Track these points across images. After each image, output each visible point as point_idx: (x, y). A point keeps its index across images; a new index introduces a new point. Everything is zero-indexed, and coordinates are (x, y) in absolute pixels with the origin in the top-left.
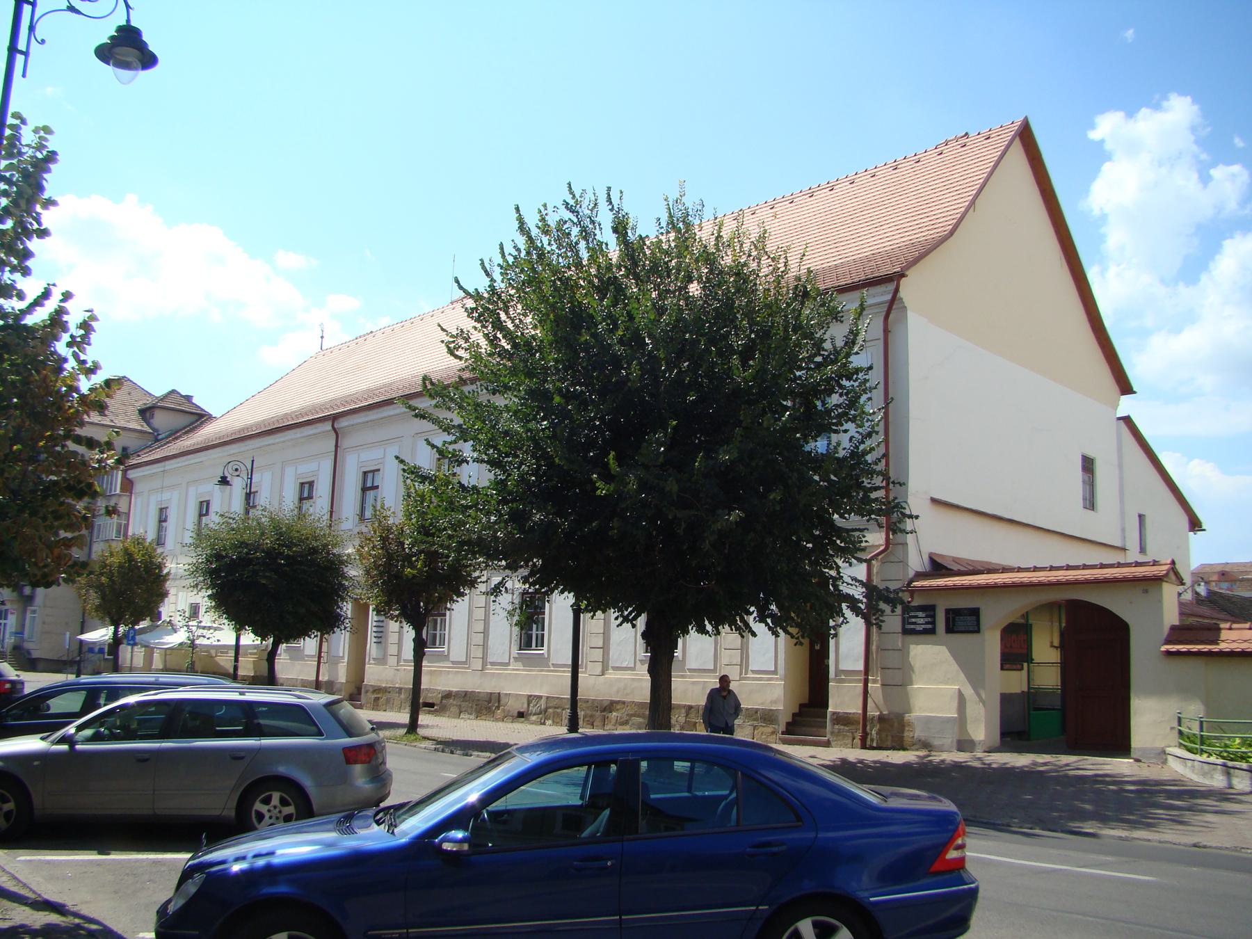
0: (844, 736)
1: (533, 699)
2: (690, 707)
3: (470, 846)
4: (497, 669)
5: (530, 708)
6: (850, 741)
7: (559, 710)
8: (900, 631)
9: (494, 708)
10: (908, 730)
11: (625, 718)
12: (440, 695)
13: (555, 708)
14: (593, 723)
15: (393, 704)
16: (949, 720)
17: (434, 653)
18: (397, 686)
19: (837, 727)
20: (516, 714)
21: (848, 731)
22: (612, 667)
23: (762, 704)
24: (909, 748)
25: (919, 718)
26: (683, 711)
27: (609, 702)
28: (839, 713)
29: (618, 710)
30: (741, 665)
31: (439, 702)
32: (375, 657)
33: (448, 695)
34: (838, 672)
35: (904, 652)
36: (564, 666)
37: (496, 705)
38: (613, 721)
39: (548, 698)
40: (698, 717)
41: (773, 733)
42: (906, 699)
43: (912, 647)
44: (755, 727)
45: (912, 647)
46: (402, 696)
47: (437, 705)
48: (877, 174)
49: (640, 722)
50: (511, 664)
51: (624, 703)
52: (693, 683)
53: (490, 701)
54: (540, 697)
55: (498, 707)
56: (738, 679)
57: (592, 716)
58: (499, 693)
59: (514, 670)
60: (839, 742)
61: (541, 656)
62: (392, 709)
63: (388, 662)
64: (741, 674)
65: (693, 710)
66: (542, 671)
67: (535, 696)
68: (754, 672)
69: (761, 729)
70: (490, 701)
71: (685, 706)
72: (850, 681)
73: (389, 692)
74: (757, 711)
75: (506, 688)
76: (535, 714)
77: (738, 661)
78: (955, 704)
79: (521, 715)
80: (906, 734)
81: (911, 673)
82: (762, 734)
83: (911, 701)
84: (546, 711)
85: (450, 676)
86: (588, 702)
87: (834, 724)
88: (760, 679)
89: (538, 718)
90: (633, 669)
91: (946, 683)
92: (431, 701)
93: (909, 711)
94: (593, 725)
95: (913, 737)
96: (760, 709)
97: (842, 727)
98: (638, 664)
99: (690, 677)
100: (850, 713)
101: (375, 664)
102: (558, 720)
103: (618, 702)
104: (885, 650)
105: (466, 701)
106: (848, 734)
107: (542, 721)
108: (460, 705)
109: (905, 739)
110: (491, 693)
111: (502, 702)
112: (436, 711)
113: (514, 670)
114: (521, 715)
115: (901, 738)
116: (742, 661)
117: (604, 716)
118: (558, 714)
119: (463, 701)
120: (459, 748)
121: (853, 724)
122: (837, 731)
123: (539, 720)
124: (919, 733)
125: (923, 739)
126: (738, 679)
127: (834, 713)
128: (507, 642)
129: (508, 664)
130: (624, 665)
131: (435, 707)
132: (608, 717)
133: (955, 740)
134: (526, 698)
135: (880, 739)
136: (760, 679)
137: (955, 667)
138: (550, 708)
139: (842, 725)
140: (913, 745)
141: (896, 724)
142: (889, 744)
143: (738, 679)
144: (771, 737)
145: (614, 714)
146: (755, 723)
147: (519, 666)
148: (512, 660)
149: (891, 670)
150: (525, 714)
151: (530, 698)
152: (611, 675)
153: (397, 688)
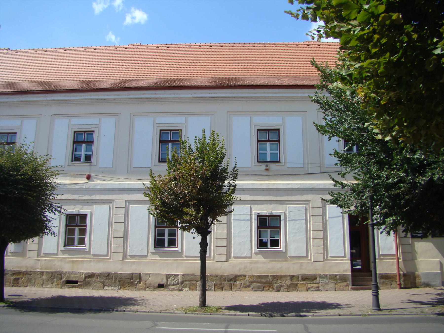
0: (386, 284)
1: (171, 276)
2: (293, 276)
3: (356, 251)
4: (136, 259)
5: (169, 282)
6: (389, 286)
7: (194, 282)
8: (410, 236)
9: (136, 283)
10: (418, 279)
11: (247, 284)
12: (83, 276)
13: (190, 281)
14: (222, 288)
15: (35, 282)
16: (437, 273)
17: (75, 250)
18: (38, 270)
19: (382, 280)
20: (156, 285)
21: (388, 282)
22: (234, 257)
23: (338, 272)
24: (419, 287)
25: (423, 274)
26: (289, 278)
27: (234, 276)
28: (382, 274)
29: (240, 280)
30: (324, 254)
31: (82, 280)
32: (12, 251)
33: (92, 275)
34: (380, 255)
35: (412, 246)
36: (195, 257)
37: (138, 280)
38: (238, 286)
39: (183, 275)
40: (299, 280)
41: (347, 285)
42: (415, 266)
43: (416, 243)
44: (335, 284)
45: (416, 243)
46: (44, 277)
47: (80, 282)
48: (87, 49)
49: (259, 286)
50: (149, 256)
51: (245, 276)
52: (294, 264)
53: (132, 278)
54: (178, 275)
55: (140, 282)
56: (323, 261)
57: (221, 284)
58: (140, 274)
59: (152, 259)
60: (384, 287)
61: (177, 252)
62: (33, 285)
63: (28, 255)
64: (324, 258)
65: (294, 277)
66: (177, 260)
67: (172, 275)
68: (331, 257)
69: (339, 284)
70: (132, 278)
71: (289, 276)
72: (386, 259)
73: (31, 274)
74: (336, 276)
75: (144, 270)
76: (173, 285)
77: (323, 252)
78: (439, 267)
79: (161, 286)
80: (417, 281)
81: (416, 254)
82: (340, 286)
83: (417, 267)
84: (182, 283)
85: (92, 264)
86: (217, 276)
87: (380, 279)
88: (336, 260)
89: (176, 287)
90: (251, 257)
91: (433, 258)
92: (74, 280)
93: (417, 270)
94: (222, 289)
95: (421, 282)
96: (337, 275)
97: (385, 280)
98: (254, 255)
99: (291, 261)
100: (388, 274)
101: (13, 256)
102: (194, 288)
103: (241, 276)
104: (404, 245)
105: (109, 279)
106: (388, 283)
107: (180, 289)
108: (103, 282)
109: (417, 283)
110: (133, 274)
111: (142, 279)
112: (79, 285)
113: (152, 259)
114: (161, 286)
115: (415, 283)
116: (324, 252)
117: (231, 283)
118: (193, 284)
119: (106, 279)
120: (435, 180)
121: (390, 278)
122: (382, 282)
123: (177, 288)
124: (423, 280)
125: (426, 282)
126: (323, 260)
127: (380, 274)
128: (145, 243)
129: (147, 256)
130: (244, 255)
131: (79, 283)
132: (234, 284)
133: (441, 282)
134: (165, 276)
135: (405, 284)
136: (336, 260)
137: (437, 251)
138: (186, 281)
139: (384, 279)
140: (421, 285)
141: (412, 277)
142: (409, 286)
143: (323, 260)
144: (346, 287)
145: (238, 282)
146: (336, 282)
147: (157, 257)
148: (150, 254)
149: (407, 254)
150: (164, 285)
151: (168, 276)
152: (233, 261)
153: (38, 272)
